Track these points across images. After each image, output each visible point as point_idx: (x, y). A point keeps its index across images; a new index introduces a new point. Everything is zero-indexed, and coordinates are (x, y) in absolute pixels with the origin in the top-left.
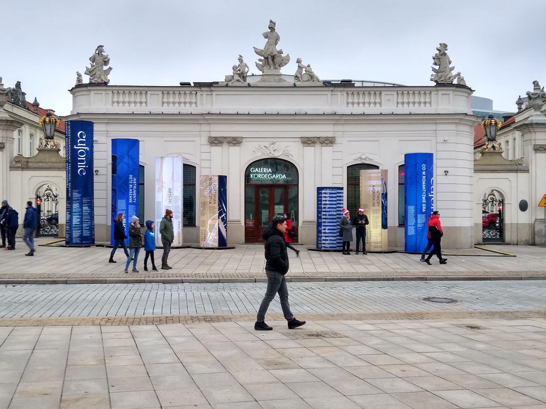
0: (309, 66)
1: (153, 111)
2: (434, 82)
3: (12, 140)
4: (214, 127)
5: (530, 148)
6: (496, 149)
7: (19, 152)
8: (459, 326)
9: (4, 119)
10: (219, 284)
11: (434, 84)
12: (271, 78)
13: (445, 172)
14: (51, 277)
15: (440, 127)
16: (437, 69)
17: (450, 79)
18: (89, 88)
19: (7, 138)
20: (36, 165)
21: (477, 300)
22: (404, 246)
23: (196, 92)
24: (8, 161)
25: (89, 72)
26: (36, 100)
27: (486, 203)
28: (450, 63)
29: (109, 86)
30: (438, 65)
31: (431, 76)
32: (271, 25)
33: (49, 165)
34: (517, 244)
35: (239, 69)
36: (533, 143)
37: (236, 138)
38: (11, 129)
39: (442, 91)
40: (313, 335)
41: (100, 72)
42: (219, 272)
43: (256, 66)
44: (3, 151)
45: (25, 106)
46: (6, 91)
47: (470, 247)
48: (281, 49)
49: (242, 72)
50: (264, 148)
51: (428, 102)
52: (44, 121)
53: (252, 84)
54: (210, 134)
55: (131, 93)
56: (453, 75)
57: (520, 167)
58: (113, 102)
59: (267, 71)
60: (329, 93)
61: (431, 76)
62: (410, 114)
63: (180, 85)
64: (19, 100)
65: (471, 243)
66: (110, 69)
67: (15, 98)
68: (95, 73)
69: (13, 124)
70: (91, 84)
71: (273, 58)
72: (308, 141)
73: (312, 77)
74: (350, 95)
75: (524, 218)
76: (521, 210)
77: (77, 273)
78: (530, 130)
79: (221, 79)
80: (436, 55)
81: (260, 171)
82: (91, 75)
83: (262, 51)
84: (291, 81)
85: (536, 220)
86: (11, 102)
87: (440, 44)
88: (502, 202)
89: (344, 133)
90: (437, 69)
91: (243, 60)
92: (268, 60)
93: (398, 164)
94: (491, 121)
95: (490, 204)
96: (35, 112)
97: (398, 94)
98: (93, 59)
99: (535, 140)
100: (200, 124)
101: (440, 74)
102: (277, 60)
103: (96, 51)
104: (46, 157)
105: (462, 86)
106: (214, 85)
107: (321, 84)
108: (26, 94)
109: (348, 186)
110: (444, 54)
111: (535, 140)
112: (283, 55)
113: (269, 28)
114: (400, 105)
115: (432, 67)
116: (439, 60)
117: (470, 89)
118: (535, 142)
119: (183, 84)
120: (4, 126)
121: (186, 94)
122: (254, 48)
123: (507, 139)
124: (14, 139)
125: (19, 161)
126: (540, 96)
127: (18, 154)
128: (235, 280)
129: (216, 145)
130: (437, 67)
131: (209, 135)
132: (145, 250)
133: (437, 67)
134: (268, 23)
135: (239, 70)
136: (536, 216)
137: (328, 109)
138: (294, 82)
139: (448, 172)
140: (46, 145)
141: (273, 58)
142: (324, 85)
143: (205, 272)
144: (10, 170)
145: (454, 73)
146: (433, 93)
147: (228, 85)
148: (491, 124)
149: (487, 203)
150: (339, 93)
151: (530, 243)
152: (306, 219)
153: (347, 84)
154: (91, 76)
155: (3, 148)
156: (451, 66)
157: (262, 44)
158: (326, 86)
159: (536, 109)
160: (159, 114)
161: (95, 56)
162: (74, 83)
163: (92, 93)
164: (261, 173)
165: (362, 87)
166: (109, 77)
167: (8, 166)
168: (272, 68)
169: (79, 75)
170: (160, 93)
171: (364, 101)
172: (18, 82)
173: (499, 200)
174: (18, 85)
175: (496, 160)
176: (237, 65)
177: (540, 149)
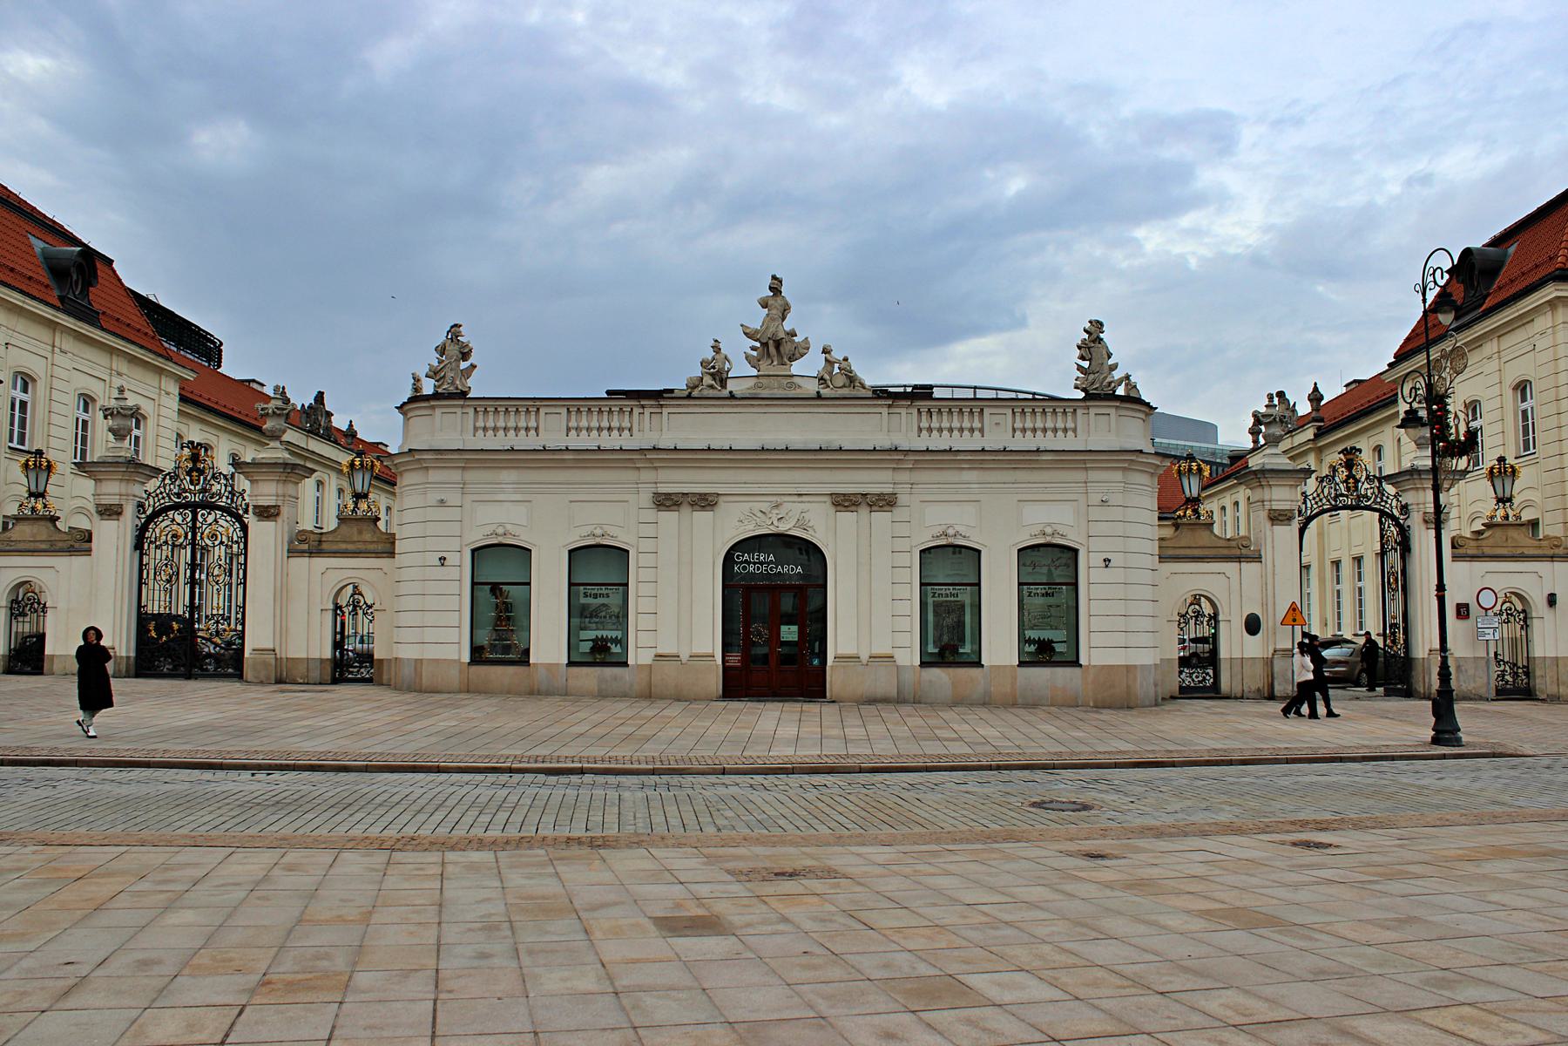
0: (846, 359)
1: (551, 445)
2: (1082, 390)
4: (663, 475)
5: (1263, 515)
6: (1202, 518)
7: (317, 523)
8: (1070, 854)
9: (281, 461)
10: (651, 777)
11: (1081, 395)
12: (774, 382)
13: (1105, 560)
14: (338, 758)
15: (471, 476)
16: (1087, 367)
17: (1109, 386)
18: (433, 403)
19: (284, 496)
20: (335, 547)
21: (1131, 804)
22: (1331, 702)
23: (632, 409)
24: (286, 539)
25: (434, 373)
26: (351, 425)
28: (1109, 357)
29: (470, 398)
31: (1076, 380)
32: (774, 284)
33: (360, 546)
34: (1242, 698)
35: (712, 364)
36: (1267, 507)
37: (706, 494)
38: (292, 479)
39: (1096, 408)
40: (783, 874)
41: (453, 372)
42: (656, 754)
43: (746, 358)
45: (329, 435)
47: (1154, 703)
48: (793, 329)
49: (718, 371)
50: (759, 514)
51: (1029, 429)
52: (352, 465)
53: (738, 394)
54: (657, 488)
55: (530, 412)
56: (1116, 378)
57: (1244, 551)
58: (476, 429)
59: (766, 367)
60: (885, 411)
61: (1076, 380)
62: (983, 450)
63: (606, 396)
64: (320, 425)
65: (1156, 696)
66: (473, 367)
67: (312, 423)
69: (297, 471)
70: (436, 396)
71: (778, 344)
72: (844, 502)
73: (852, 380)
74: (1018, 415)
75: (1254, 647)
77: (473, 753)
78: (1260, 482)
79: (679, 384)
81: (753, 559)
82: (438, 378)
83: (757, 331)
84: (812, 387)
86: (305, 430)
87: (1090, 322)
88: (1214, 618)
89: (914, 486)
90: (1087, 367)
91: (720, 349)
92: (768, 348)
94: (1190, 466)
95: (1192, 622)
96: (349, 447)
97: (1014, 413)
98: (442, 350)
99: (1270, 501)
100: (638, 468)
101: (1091, 377)
102: (786, 348)
103: (448, 334)
104: (351, 531)
105: (1133, 400)
106: (665, 395)
107: (870, 394)
108: (332, 415)
109: (821, 582)
111: (1270, 501)
113: (771, 288)
114: (1018, 433)
117: (1148, 404)
120: (278, 474)
122: (742, 325)
123: (1235, 498)
126: (1278, 420)
127: (315, 527)
128: (684, 769)
129: (668, 508)
130: (1086, 364)
131: (654, 490)
132: (1433, 730)
133: (1086, 364)
134: (769, 281)
135: (714, 367)
136: (1275, 644)
137: (883, 441)
138: (817, 390)
139: (1109, 561)
140: (354, 510)
141: (778, 344)
142: (874, 396)
143: (602, 753)
145: (1117, 375)
146: (1079, 412)
147: (692, 396)
148: (1190, 470)
150: (903, 411)
151: (1266, 695)
152: (841, 651)
153: (921, 394)
154: (437, 381)
155: (278, 514)
156: (1111, 362)
157: (757, 318)
158: (879, 398)
160: (561, 450)
161: (445, 344)
162: (408, 393)
163: (438, 412)
164: (755, 563)
165: (975, 399)
166: (470, 382)
167: (286, 548)
168: (775, 363)
169: (416, 380)
171: (972, 426)
172: (319, 392)
173: (1209, 615)
174: (320, 397)
175: (1202, 537)
176: (710, 359)
177: (1280, 518)
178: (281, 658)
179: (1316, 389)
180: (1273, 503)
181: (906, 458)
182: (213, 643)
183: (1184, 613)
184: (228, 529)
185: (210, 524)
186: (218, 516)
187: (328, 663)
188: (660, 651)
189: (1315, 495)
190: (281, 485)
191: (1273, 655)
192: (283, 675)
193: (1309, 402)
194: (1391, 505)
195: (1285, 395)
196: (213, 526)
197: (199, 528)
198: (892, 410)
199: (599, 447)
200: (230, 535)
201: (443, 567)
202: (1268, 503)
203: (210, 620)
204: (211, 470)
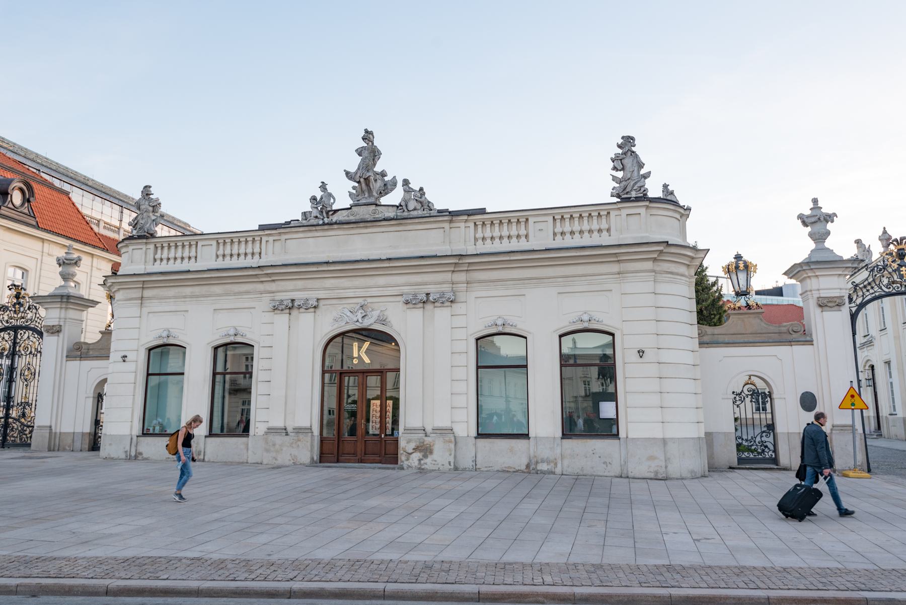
3: (80, 322)
20: (96, 354)
23: (261, 238)
27: (740, 399)
30: (620, 170)
31: (613, 189)
43: (350, 195)
44: (60, 335)
46: (73, 260)
60: (446, 225)
68: (138, 222)
69: (72, 301)
73: (428, 206)
76: (804, 410)
80: (617, 155)
85: (833, 426)
93: (558, 331)
110: (629, 153)
112: (386, 179)
115: (611, 175)
116: (621, 162)
118: (819, 294)
119: (262, 228)
121: (564, 219)
124: (82, 321)
125: (79, 348)
126: (822, 219)
130: (620, 174)
134: (363, 133)
144: (66, 361)
149: (743, 398)
150: (462, 225)
156: (643, 172)
159: (816, 240)
167: (65, 355)
170: (214, 243)
177: (829, 304)
178: (55, 433)
179: (885, 232)
180: (821, 291)
181: (461, 262)
182: (20, 422)
183: (739, 391)
184: (34, 343)
185: (25, 340)
186: (30, 334)
187: (88, 435)
188: (271, 425)
189: (40, 318)
190: (63, 311)
191: (832, 430)
192: (55, 444)
193: (880, 242)
194: (41, 325)
195: (861, 242)
196: (27, 342)
197: (18, 343)
198: (453, 225)
199: (860, 381)
200: (36, 347)
201: (124, 363)
202: (817, 292)
203: (20, 406)
204: (28, 304)
